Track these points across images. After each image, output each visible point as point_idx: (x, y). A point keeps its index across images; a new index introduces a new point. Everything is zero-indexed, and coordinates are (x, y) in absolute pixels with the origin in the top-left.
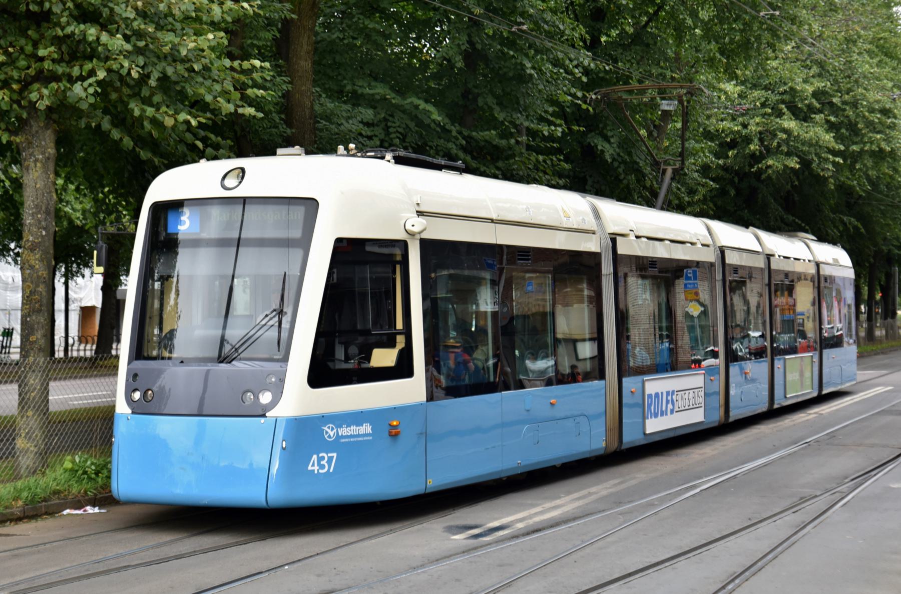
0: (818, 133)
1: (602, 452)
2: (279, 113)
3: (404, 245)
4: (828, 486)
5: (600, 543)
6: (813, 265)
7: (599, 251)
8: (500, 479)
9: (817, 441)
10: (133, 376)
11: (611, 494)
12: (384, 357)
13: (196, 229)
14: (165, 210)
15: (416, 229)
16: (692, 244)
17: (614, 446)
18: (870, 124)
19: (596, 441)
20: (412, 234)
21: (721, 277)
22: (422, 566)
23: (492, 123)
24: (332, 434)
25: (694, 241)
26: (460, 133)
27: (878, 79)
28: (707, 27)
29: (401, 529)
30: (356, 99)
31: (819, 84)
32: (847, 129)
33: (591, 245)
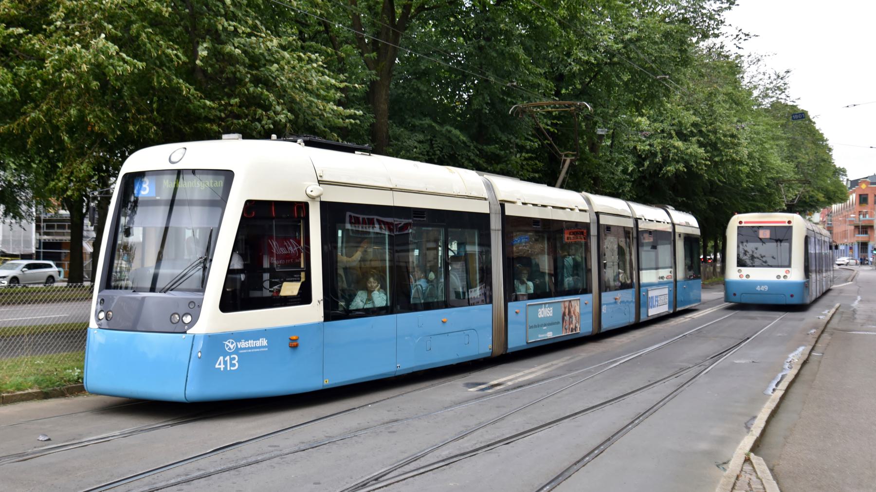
0: (694, 149)
1: (489, 355)
2: (368, 135)
3: (303, 207)
4: (697, 362)
5: (558, 395)
6: (670, 225)
7: (588, 221)
8: (452, 365)
9: (690, 334)
10: (102, 301)
11: (565, 365)
12: (290, 289)
13: (153, 195)
14: (132, 179)
15: (314, 194)
16: (572, 209)
17: (596, 332)
18: (725, 144)
19: (484, 346)
20: (313, 198)
21: (596, 234)
22: (451, 407)
23: (497, 141)
24: (232, 347)
25: (573, 207)
26: (476, 147)
27: (728, 116)
28: (626, 84)
29: (438, 384)
30: (413, 129)
31: (694, 118)
32: (712, 146)
33: (482, 208)
